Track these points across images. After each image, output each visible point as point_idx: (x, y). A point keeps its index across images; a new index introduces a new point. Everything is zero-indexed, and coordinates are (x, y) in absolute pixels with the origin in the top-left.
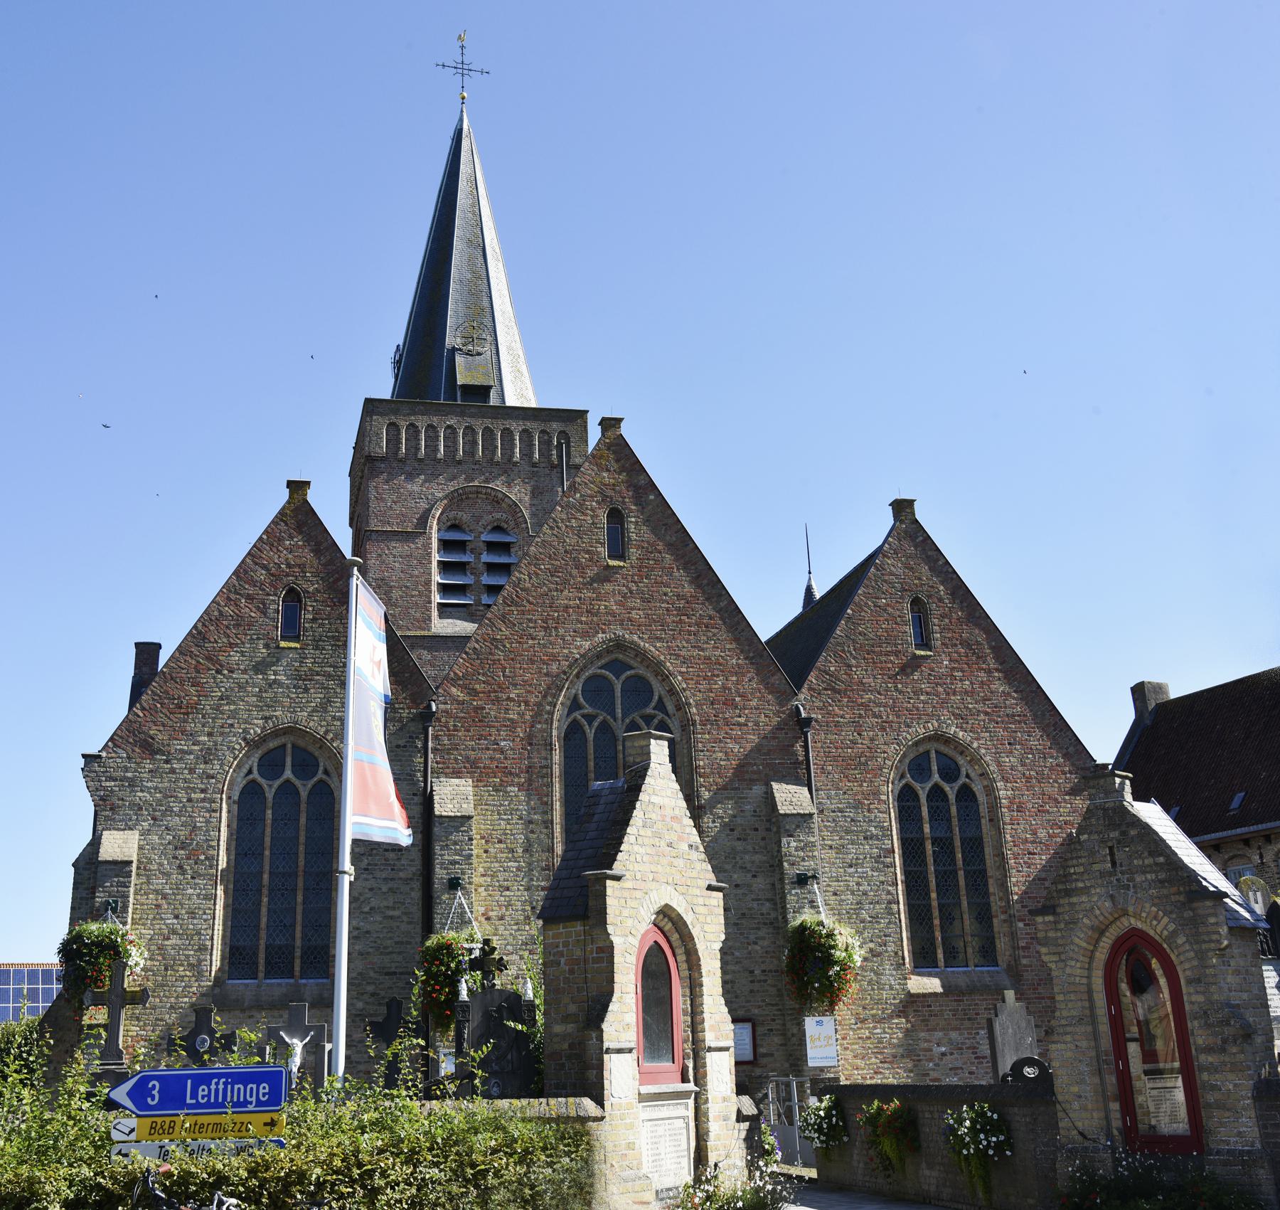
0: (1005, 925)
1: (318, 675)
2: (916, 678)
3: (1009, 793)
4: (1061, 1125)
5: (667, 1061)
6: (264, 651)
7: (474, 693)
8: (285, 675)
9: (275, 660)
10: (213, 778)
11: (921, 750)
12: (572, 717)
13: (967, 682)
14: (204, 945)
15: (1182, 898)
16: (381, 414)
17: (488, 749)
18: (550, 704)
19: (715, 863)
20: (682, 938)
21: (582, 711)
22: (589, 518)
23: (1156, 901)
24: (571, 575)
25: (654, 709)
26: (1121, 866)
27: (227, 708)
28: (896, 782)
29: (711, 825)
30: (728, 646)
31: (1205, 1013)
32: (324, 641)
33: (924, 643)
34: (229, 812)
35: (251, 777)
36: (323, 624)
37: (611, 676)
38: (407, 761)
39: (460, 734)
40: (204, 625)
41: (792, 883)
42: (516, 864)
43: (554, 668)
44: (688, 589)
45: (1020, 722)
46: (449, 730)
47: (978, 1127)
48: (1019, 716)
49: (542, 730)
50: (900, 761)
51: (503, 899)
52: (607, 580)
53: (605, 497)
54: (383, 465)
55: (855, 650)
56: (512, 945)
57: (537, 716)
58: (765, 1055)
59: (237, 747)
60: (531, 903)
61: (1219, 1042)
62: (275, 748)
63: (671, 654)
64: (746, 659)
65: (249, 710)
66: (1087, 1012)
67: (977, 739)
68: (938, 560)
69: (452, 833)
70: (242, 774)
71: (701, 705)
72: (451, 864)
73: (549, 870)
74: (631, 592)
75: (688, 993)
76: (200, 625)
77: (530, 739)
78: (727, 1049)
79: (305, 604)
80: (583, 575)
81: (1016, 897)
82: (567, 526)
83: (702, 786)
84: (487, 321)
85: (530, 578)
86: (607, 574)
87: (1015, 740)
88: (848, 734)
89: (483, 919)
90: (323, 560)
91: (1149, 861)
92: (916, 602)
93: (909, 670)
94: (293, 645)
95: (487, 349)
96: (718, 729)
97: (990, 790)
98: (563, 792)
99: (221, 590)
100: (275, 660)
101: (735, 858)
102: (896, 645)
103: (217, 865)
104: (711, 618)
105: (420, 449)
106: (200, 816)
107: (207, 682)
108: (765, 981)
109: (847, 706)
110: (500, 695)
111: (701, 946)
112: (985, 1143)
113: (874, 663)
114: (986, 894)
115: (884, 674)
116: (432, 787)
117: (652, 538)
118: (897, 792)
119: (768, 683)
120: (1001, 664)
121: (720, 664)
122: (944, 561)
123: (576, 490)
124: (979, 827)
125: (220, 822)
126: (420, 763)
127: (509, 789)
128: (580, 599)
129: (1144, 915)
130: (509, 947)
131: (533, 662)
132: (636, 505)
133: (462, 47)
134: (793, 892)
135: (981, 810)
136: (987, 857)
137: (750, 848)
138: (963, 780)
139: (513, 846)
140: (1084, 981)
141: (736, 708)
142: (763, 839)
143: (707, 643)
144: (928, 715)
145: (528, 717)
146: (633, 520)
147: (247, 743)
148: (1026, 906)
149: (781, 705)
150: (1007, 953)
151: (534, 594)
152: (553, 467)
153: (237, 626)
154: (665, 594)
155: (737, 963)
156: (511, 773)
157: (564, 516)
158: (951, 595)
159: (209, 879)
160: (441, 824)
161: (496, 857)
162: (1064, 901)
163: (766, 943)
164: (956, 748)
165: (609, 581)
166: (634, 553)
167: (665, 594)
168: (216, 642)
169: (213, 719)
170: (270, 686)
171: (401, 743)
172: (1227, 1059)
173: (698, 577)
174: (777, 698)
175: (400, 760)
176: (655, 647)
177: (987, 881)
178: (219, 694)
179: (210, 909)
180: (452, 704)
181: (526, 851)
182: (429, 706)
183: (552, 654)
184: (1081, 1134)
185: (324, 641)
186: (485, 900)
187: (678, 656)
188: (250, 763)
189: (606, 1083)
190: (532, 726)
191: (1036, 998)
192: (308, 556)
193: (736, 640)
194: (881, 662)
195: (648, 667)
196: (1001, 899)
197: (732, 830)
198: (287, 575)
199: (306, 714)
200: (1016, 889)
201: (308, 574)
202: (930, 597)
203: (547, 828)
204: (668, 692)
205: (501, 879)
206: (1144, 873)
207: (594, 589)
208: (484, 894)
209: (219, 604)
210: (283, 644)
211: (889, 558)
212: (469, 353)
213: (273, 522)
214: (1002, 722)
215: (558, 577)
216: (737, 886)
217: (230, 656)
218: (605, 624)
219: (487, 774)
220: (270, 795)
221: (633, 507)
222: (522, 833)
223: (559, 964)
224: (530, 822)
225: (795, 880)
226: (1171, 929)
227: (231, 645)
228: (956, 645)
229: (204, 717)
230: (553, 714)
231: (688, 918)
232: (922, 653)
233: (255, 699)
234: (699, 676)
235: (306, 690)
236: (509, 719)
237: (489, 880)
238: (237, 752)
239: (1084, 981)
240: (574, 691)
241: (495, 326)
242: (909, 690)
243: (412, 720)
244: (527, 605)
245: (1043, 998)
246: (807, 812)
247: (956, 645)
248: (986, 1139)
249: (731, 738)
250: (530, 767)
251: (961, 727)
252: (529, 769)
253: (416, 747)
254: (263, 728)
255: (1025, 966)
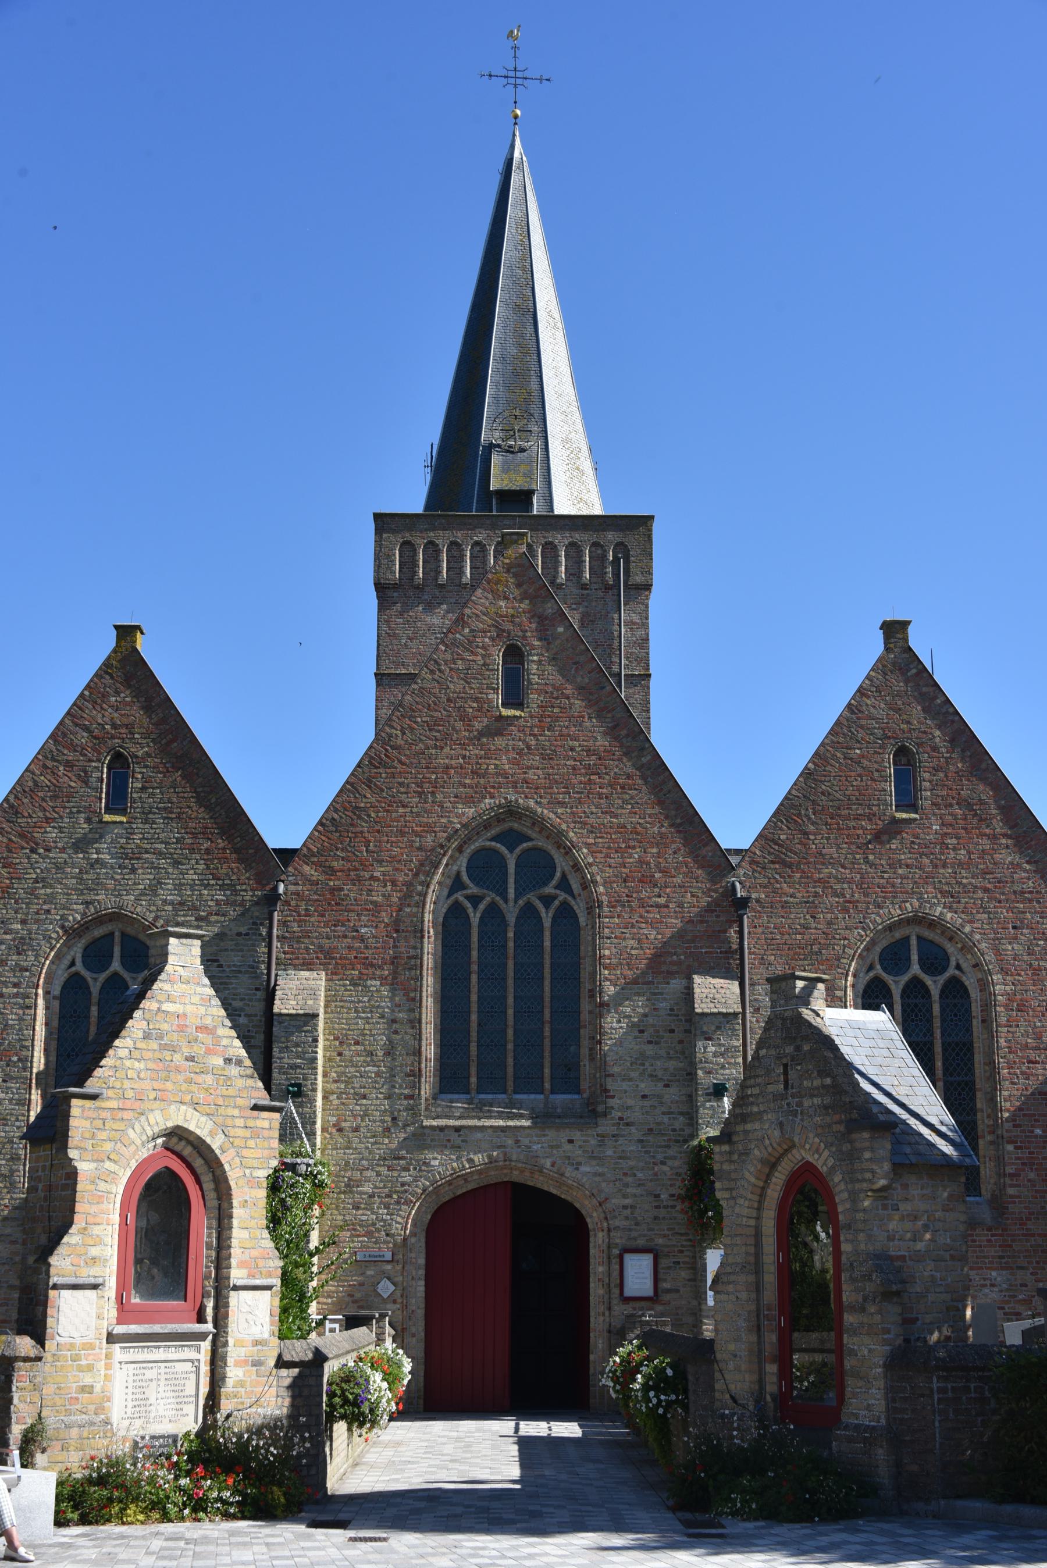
0: (992, 1147)
1: (147, 852)
2: (893, 846)
3: (1008, 988)
4: (717, 1386)
5: (177, 1298)
6: (85, 826)
7: (331, 871)
8: (109, 853)
9: (97, 836)
10: (27, 970)
11: (898, 935)
12: (453, 898)
13: (963, 852)
14: (17, 1154)
15: (841, 1128)
16: (394, 532)
17: (345, 937)
18: (422, 883)
19: (844, 1063)
20: (207, 1162)
21: (465, 892)
22: (479, 658)
23: (820, 1131)
24: (454, 729)
25: (556, 888)
26: (792, 1088)
27: (42, 891)
28: (861, 975)
29: (615, 1025)
30: (649, 811)
31: (851, 1264)
32: (155, 813)
33: (908, 800)
34: (47, 1008)
35: (73, 969)
36: (154, 794)
37: (503, 849)
38: (249, 951)
39: (312, 919)
40: (16, 797)
41: (708, 1094)
42: (375, 1069)
43: (429, 840)
44: (602, 742)
45: (1030, 901)
46: (299, 915)
47: (651, 1383)
48: (1031, 892)
49: (410, 915)
50: (867, 949)
51: (358, 1108)
52: (499, 733)
53: (500, 631)
54: (395, 594)
55: (814, 814)
56: (367, 1160)
57: (406, 897)
58: (668, 1291)
59: (54, 935)
60: (392, 1113)
61: (861, 1300)
62: (102, 937)
63: (575, 822)
64: (671, 826)
65: (68, 894)
66: (752, 1259)
67: (971, 922)
68: (936, 698)
69: (293, 1033)
70: (63, 967)
71: (610, 883)
72: (292, 1068)
73: (414, 1075)
74: (529, 748)
75: (215, 1224)
76: (12, 798)
77: (396, 926)
78: (269, 1288)
79: (134, 771)
80: (469, 727)
81: (1006, 1115)
82: (451, 669)
83: (607, 979)
84: (535, 408)
85: (404, 733)
86: (499, 726)
87: (1022, 922)
88: (800, 916)
89: (334, 1131)
90: (155, 719)
91: (817, 1083)
92: (902, 752)
93: (885, 838)
94: (118, 818)
95: (533, 444)
96: (631, 912)
97: (984, 985)
98: (439, 987)
99: (36, 757)
100: (97, 836)
101: (643, 1065)
102: (870, 806)
103: (32, 1067)
104: (629, 777)
105: (441, 572)
106: (12, 1013)
107: (21, 863)
108: (673, 1207)
109: (800, 883)
110: (362, 873)
111: (233, 1175)
112: (655, 1401)
113: (839, 829)
114: (973, 1110)
115: (851, 843)
116: (276, 980)
117: (558, 679)
118: (861, 987)
119: (697, 856)
120: (1011, 828)
121: (637, 833)
122: (943, 699)
123: (465, 624)
124: (969, 1030)
125: (35, 1020)
126: (264, 953)
127: (369, 982)
128: (464, 757)
129: (807, 1146)
130: (364, 1162)
131: (403, 834)
132: (540, 639)
133: (515, 48)
134: (708, 1105)
135: (973, 1008)
136: (976, 1066)
137: (663, 1053)
138: (951, 971)
139: (372, 1048)
140: (752, 1222)
141: (655, 886)
142: (681, 1042)
143: (622, 808)
144: (907, 892)
145: (395, 899)
146: (535, 658)
147: (66, 932)
148: (1019, 1126)
149: (713, 882)
150: (992, 1181)
151: (408, 753)
152: (607, 588)
153: (54, 797)
154: (572, 749)
155: (639, 1185)
156: (372, 965)
157: (449, 657)
158: (949, 742)
159: (23, 1083)
160: (280, 1023)
161: (351, 1061)
162: (739, 1128)
163: (677, 1163)
164: (943, 933)
165: (502, 735)
166: (534, 699)
167: (572, 749)
168: (31, 817)
169: (27, 904)
170: (92, 866)
171: (243, 930)
172: (865, 1320)
173: (615, 727)
174: (709, 874)
175: (242, 950)
176: (556, 813)
177: (975, 1095)
178: (34, 876)
179: (23, 1115)
180: (304, 885)
181: (387, 1054)
182: (276, 888)
183: (427, 825)
184: (733, 1398)
185: (155, 813)
186: (337, 1110)
187: (586, 824)
188: (72, 953)
189: (49, 1320)
190: (400, 910)
191: (1023, 1235)
192: (137, 714)
193: (660, 803)
194: (849, 828)
195: (548, 838)
196: (989, 1116)
197: (641, 1032)
198: (113, 737)
199: (133, 898)
200: (1008, 1104)
201: (136, 736)
202: (920, 745)
203: (413, 1027)
204: (573, 867)
205: (356, 1085)
206: (812, 1096)
207: (482, 745)
208: (336, 1102)
209: (33, 773)
210: (107, 818)
211: (868, 697)
212: (509, 450)
213: (96, 675)
214: (1007, 900)
215: (439, 731)
216: (644, 1097)
217: (46, 832)
218: (493, 787)
219: (344, 966)
220: (95, 990)
221: (536, 643)
222: (383, 1034)
223: (37, 1190)
224: (394, 1021)
225: (711, 1090)
226: (830, 1165)
227: (48, 820)
228: (951, 805)
229: (16, 902)
230: (425, 895)
231: (215, 1143)
232: (905, 816)
233: (74, 881)
234: (609, 848)
235: (133, 870)
236: (372, 902)
237: (342, 1086)
238: (54, 942)
239: (752, 1222)
240: (455, 868)
241: (544, 414)
242: (883, 862)
243: (257, 903)
244: (399, 766)
245: (1033, 1235)
246: (731, 1011)
247: (951, 805)
248: (657, 1396)
249: (646, 923)
250: (396, 958)
251: (950, 908)
252: (394, 960)
253: (261, 935)
254: (84, 915)
255: (1012, 1196)
